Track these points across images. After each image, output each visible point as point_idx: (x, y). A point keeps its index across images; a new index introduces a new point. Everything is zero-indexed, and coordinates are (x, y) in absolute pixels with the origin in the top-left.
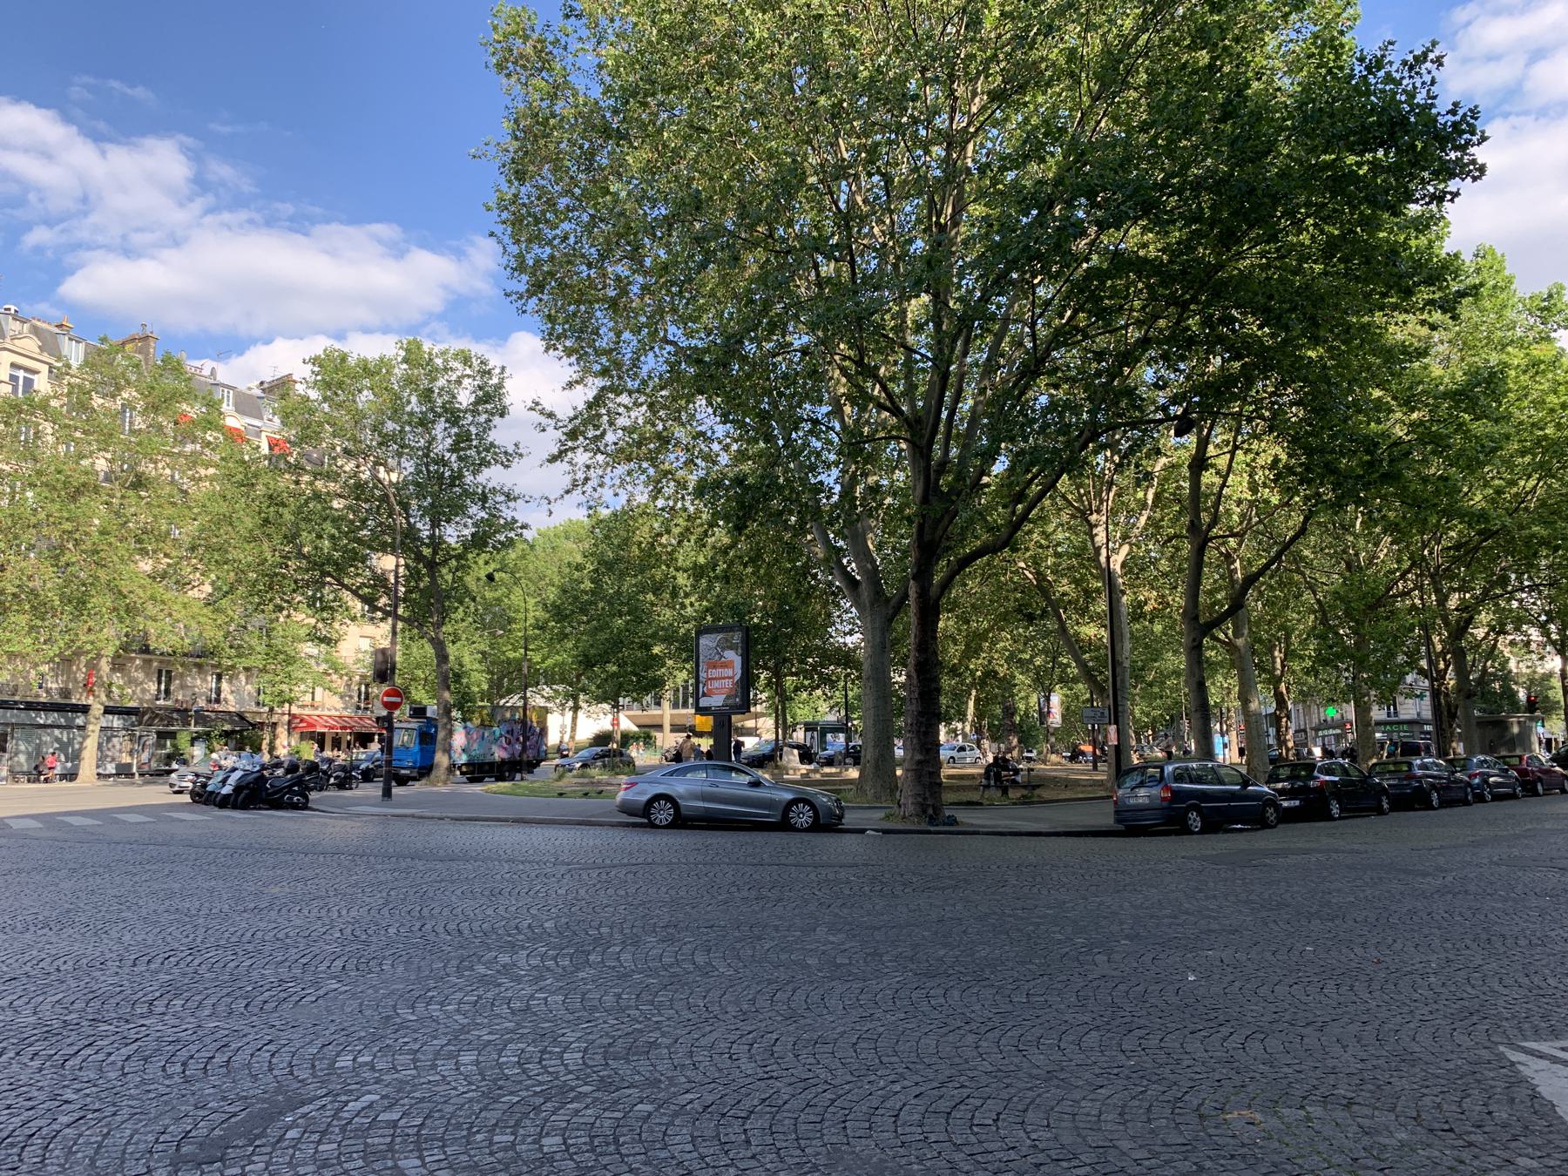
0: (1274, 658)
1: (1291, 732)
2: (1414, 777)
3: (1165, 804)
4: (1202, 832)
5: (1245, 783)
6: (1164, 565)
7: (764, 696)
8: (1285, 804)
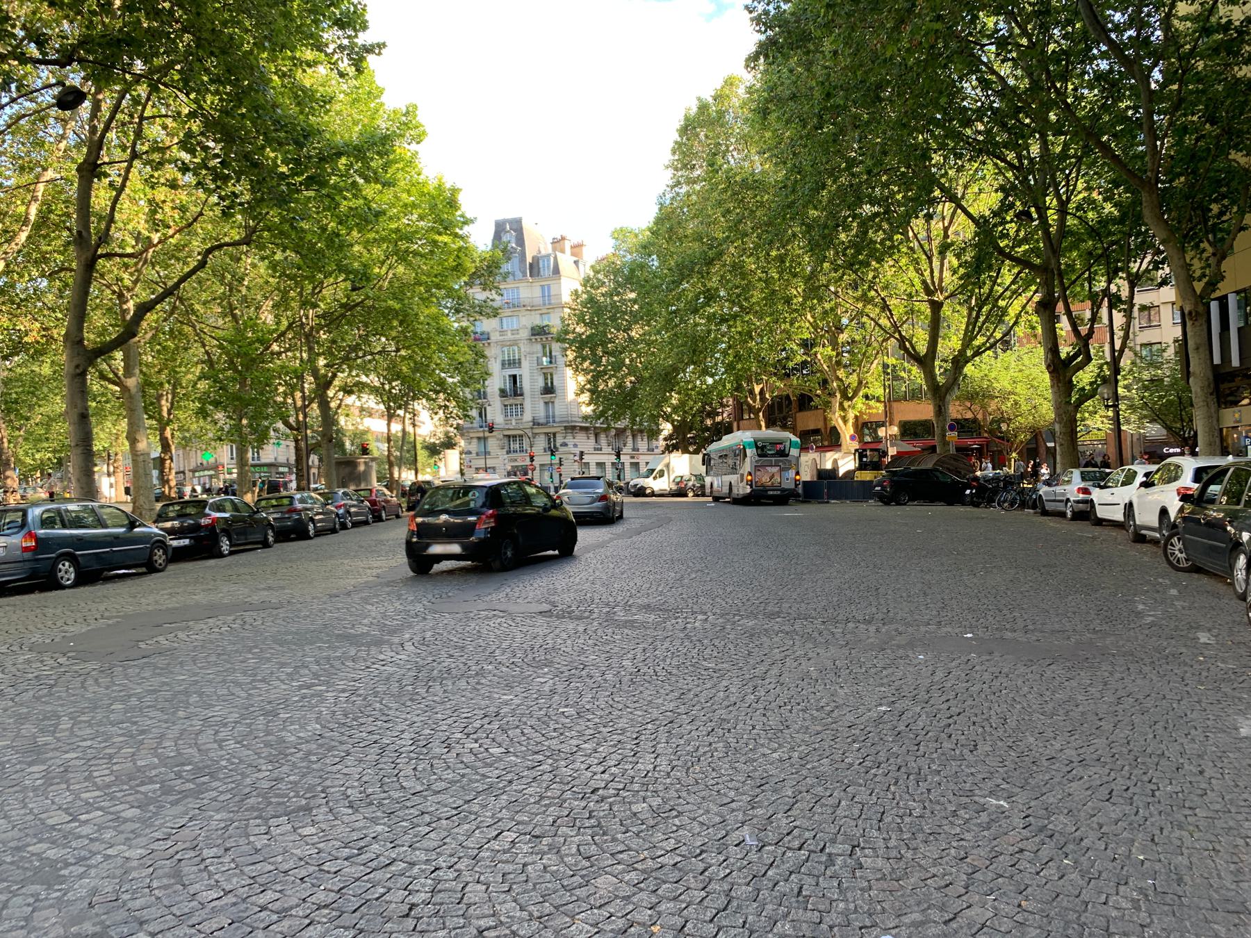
0: (160, 406)
1: (173, 472)
2: (295, 511)
3: (28, 555)
4: (77, 583)
5: (132, 525)
6: (50, 298)
7: (113, 495)
8: (175, 543)
